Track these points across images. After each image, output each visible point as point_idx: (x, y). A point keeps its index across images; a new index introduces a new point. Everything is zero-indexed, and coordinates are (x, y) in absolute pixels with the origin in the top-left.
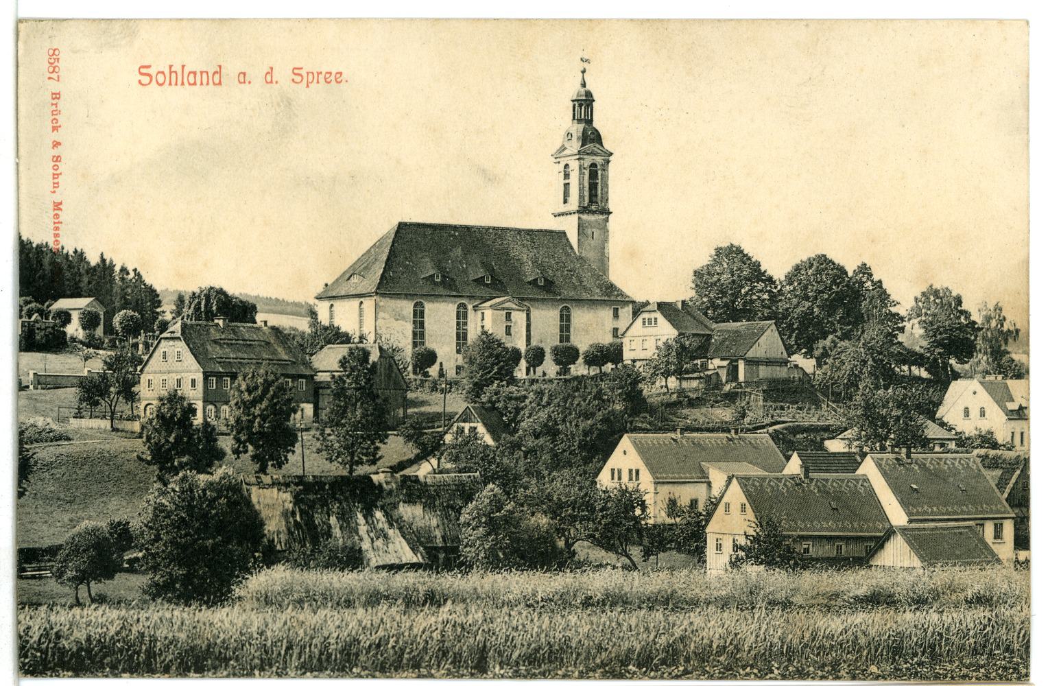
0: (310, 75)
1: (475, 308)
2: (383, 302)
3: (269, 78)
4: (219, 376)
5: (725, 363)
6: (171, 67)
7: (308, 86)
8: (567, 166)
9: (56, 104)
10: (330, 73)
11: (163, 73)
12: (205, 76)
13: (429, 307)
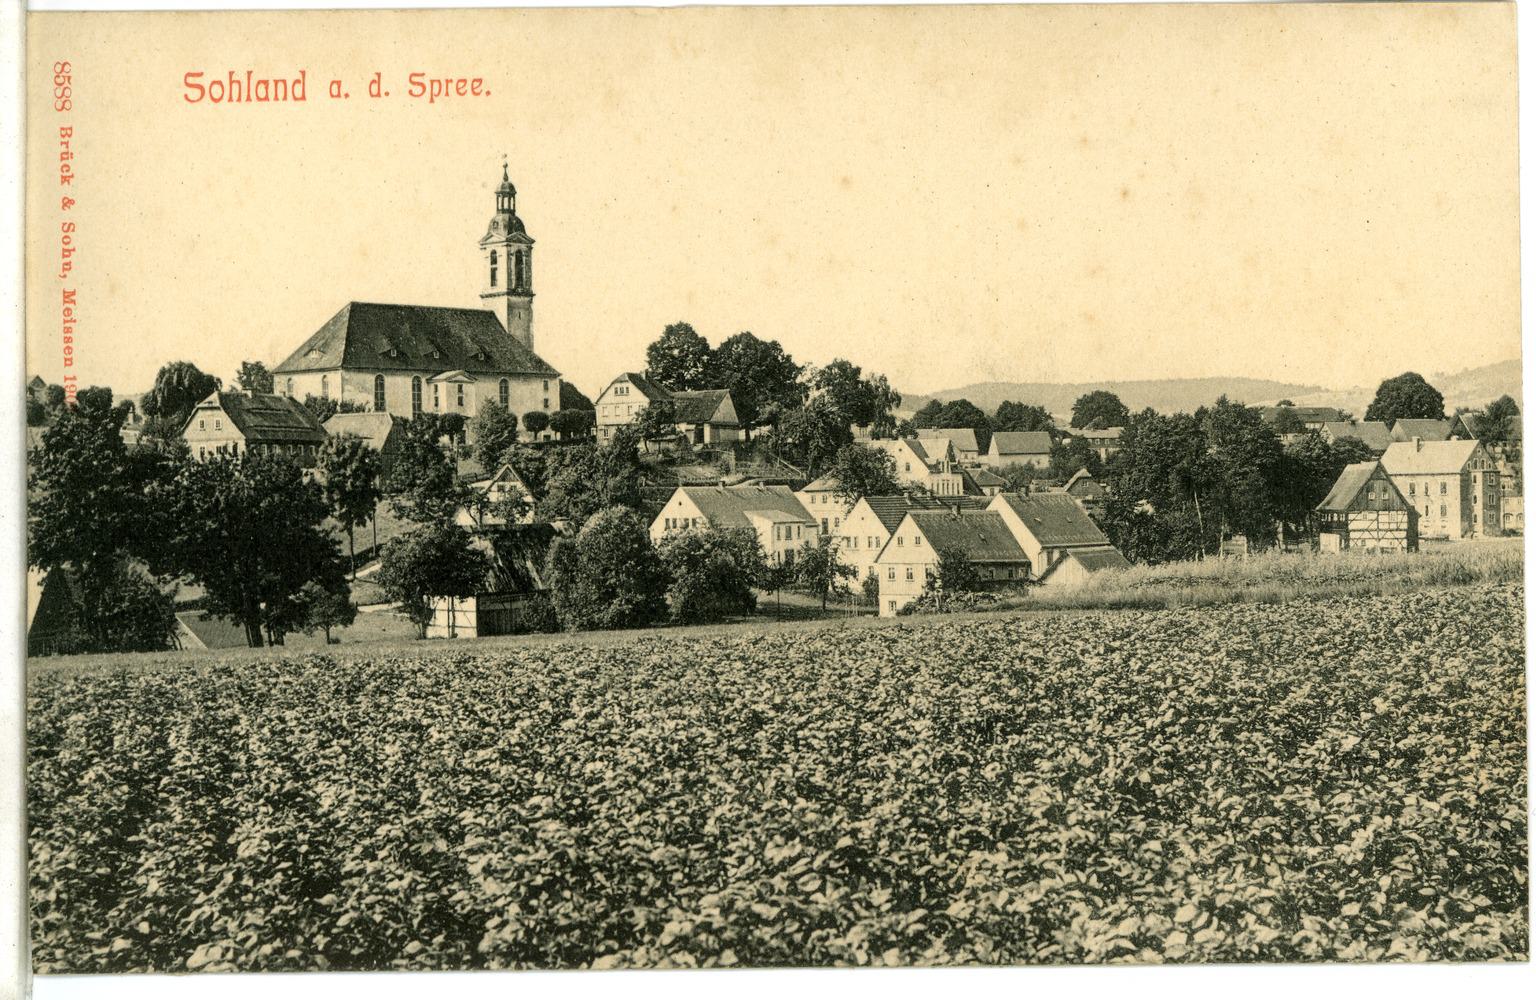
0: (436, 85)
1: (429, 381)
2: (347, 376)
3: (374, 88)
4: (259, 443)
5: (693, 427)
6: (231, 73)
7: (432, 101)
8: (494, 252)
9: (67, 143)
10: (465, 81)
11: (220, 83)
12: (281, 86)
13: (388, 380)
